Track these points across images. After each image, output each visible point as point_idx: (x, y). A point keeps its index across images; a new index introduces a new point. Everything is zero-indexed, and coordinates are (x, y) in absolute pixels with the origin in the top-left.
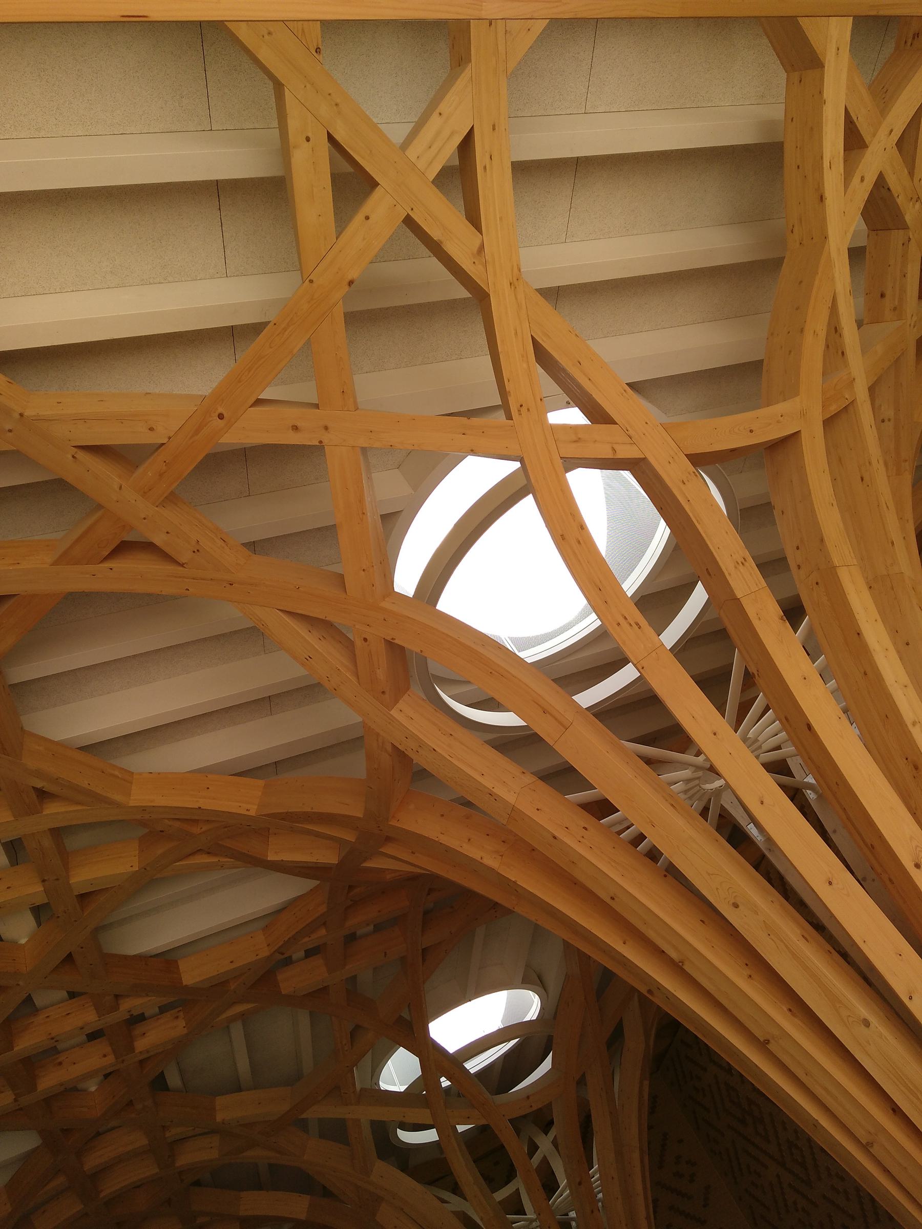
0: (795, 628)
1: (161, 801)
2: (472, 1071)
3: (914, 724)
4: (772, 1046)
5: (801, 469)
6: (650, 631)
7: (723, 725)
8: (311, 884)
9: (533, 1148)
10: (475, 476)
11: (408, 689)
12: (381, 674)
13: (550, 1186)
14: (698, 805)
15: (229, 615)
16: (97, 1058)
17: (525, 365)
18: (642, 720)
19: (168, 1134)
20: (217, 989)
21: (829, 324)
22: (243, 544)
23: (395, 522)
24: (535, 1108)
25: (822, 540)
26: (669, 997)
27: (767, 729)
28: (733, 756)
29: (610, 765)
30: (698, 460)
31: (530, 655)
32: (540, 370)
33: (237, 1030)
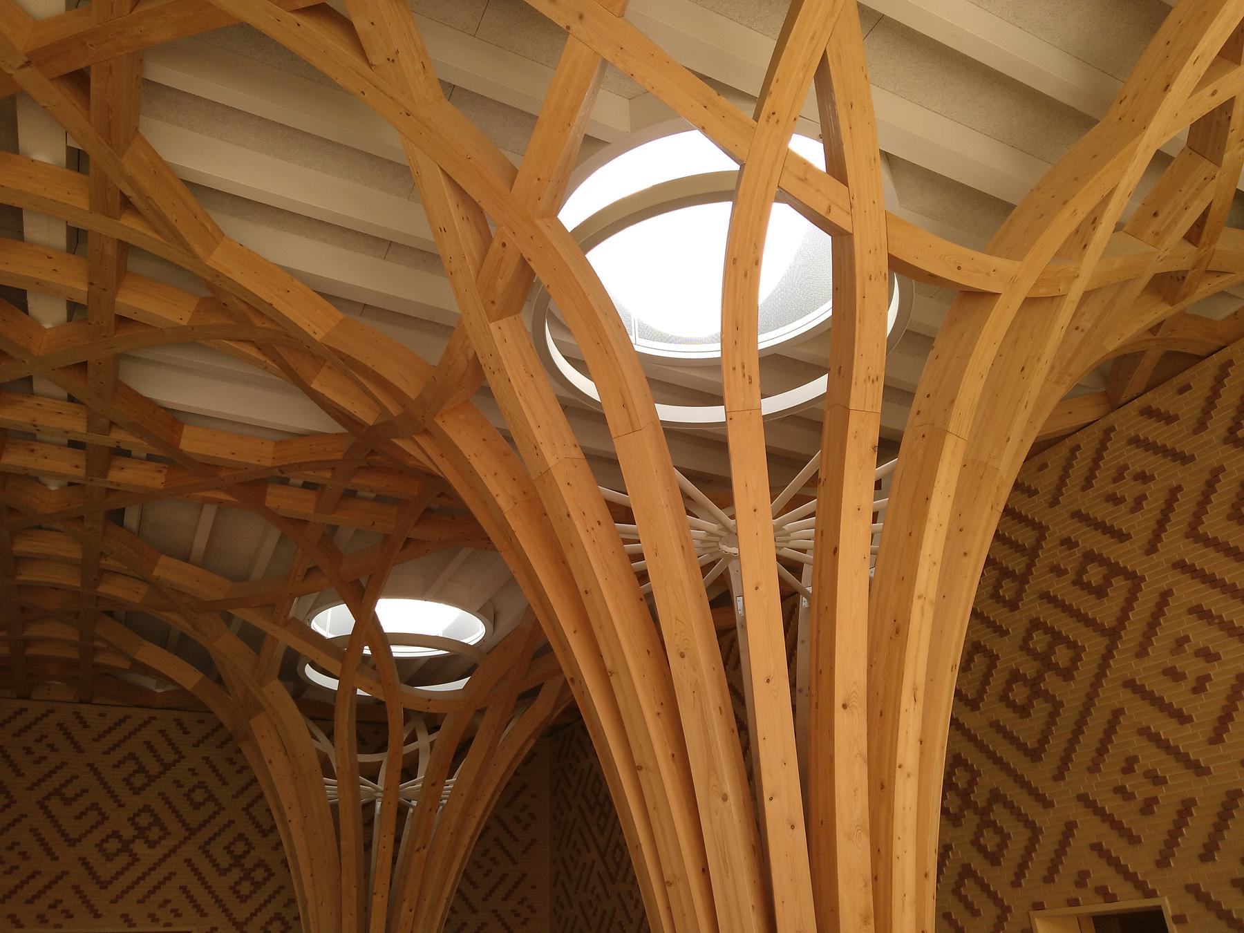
0: (880, 462)
1: (238, 276)
2: (395, 655)
3: (920, 597)
4: (641, 774)
5: (979, 328)
6: (758, 392)
7: (766, 507)
8: (339, 429)
9: (413, 738)
10: (690, 153)
11: (518, 312)
12: (501, 284)
13: (409, 772)
14: (706, 558)
15: (390, 142)
16: (69, 465)
17: (801, 75)
18: (703, 465)
19: (103, 561)
20: (208, 469)
21: (1093, 211)
22: (440, 81)
23: (596, 149)
24: (430, 711)
25: (953, 402)
26: (584, 692)
27: (801, 530)
28: (757, 535)
29: (652, 481)
30: (897, 265)
31: (643, 346)
32: (813, 87)
33: (209, 512)
